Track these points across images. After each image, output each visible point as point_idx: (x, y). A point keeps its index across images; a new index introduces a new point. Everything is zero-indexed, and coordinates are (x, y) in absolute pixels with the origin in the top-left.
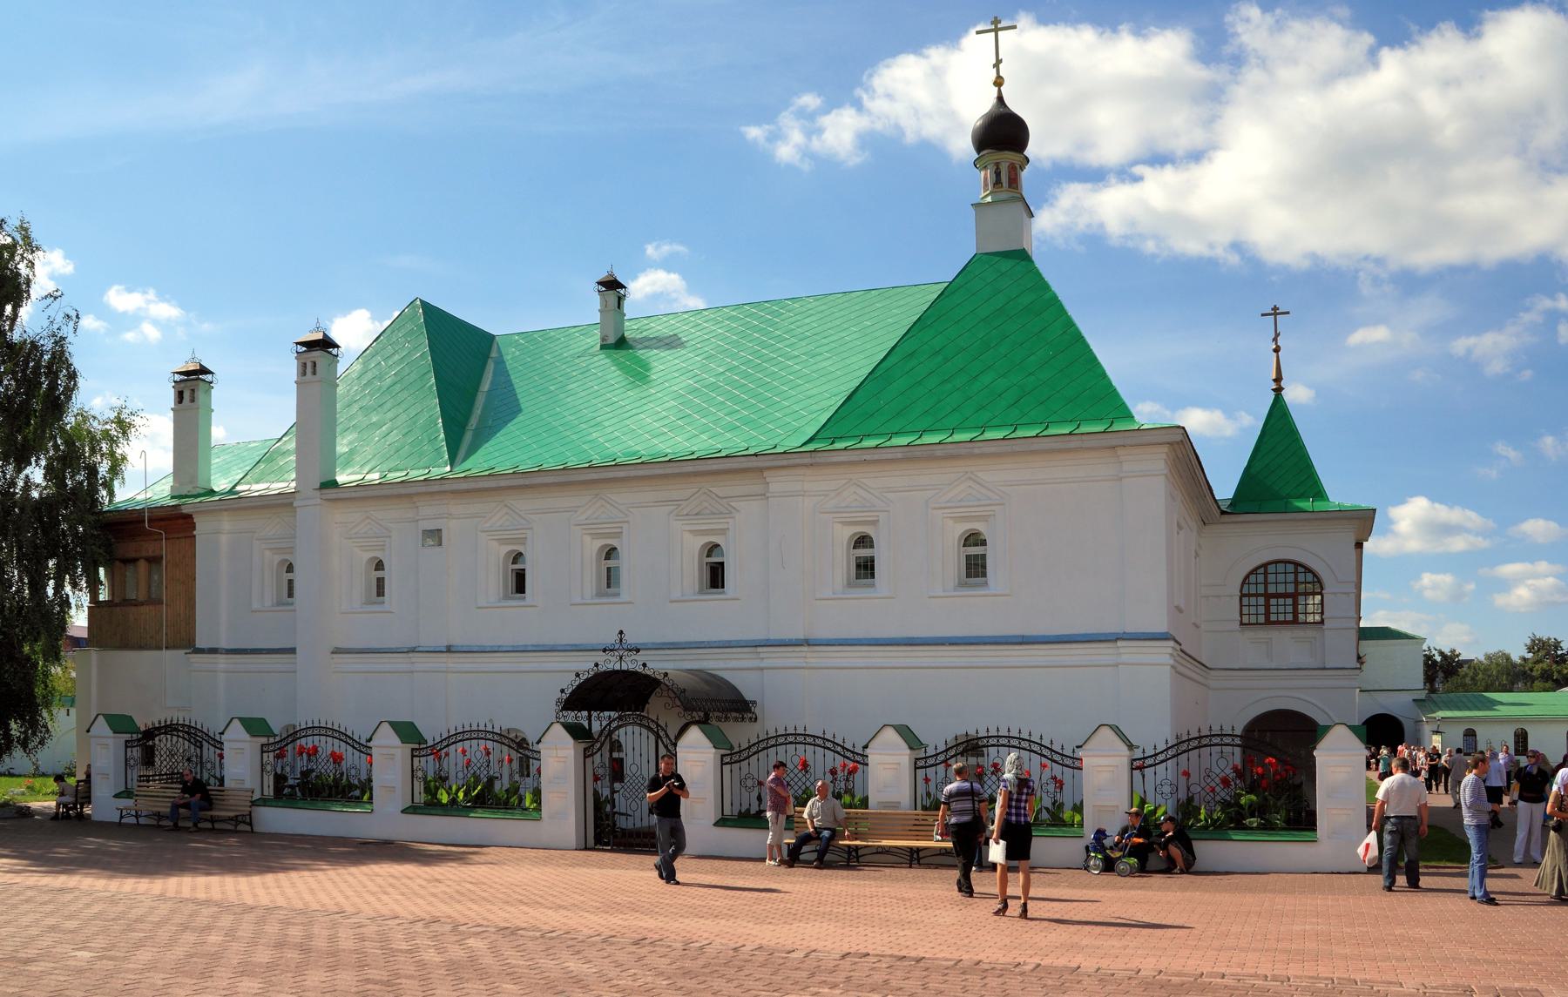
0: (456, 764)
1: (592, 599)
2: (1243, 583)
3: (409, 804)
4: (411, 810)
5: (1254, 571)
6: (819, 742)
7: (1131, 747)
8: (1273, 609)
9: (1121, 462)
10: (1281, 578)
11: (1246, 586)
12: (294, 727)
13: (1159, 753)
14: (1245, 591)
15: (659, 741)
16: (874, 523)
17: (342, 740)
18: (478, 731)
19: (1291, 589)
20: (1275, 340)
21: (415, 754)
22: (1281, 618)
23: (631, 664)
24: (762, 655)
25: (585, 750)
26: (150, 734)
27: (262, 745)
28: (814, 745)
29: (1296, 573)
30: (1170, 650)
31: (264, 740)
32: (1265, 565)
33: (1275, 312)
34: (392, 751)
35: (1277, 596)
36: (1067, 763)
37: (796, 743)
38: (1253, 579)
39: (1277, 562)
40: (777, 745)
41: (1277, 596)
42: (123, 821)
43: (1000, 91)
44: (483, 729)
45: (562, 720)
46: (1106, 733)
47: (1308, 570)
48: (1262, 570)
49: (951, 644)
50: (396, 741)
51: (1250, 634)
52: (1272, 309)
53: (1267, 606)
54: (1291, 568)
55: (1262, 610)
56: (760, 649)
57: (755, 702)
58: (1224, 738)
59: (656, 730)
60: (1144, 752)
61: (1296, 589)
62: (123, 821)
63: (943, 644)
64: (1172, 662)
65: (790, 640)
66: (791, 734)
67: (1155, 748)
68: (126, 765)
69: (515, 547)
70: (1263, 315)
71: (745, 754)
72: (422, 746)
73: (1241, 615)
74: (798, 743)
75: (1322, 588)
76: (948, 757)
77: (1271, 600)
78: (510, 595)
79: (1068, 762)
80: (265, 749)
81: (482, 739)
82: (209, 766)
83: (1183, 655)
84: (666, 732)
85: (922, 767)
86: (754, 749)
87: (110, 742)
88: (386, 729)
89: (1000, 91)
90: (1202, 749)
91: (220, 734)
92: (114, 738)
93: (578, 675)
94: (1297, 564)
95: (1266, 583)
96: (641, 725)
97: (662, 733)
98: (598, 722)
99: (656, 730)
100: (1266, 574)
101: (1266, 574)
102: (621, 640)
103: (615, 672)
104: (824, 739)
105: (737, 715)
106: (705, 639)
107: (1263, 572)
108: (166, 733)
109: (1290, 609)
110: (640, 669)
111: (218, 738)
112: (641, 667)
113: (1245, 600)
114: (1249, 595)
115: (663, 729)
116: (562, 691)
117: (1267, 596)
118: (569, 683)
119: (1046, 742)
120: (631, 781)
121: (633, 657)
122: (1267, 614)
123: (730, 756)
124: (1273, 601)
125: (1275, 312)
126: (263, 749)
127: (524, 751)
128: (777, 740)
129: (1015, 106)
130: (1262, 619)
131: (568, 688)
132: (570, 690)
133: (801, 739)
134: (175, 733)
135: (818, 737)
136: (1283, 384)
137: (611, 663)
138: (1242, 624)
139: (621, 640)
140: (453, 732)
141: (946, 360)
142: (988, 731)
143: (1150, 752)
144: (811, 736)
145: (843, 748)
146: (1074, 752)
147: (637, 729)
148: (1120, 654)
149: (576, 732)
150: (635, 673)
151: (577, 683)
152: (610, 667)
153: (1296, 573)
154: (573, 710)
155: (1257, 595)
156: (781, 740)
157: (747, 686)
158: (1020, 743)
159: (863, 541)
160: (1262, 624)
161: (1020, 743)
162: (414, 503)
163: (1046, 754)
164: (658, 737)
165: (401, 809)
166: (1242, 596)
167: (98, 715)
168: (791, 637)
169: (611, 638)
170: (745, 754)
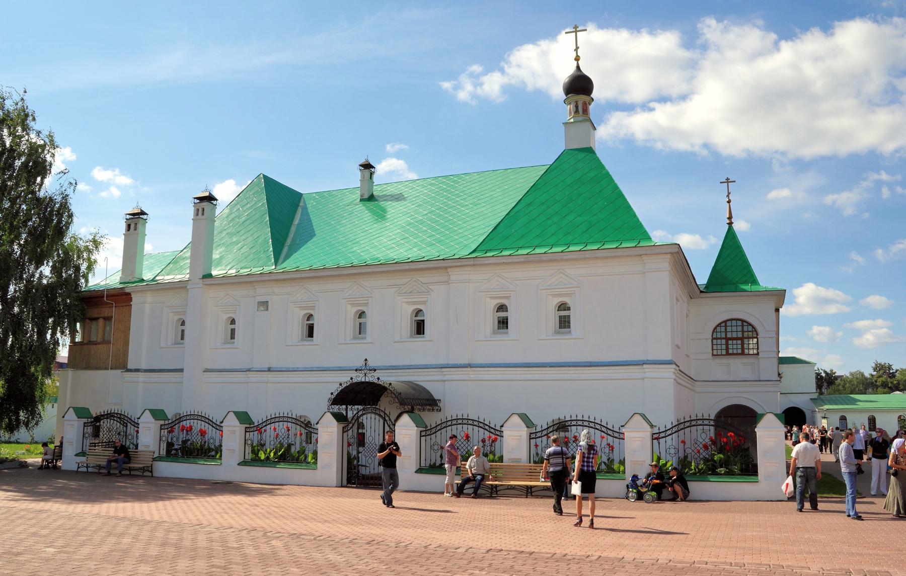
0: (270, 437)
4: (243, 464)
6: (476, 423)
8: (730, 347)
12: (180, 414)
13: (543, 430)
14: (715, 336)
16: (508, 298)
17: (481, 427)
19: (740, 335)
20: (728, 196)
22: (735, 351)
24: (444, 373)
27: (161, 425)
29: (743, 326)
30: (673, 370)
31: (162, 422)
32: (725, 322)
33: (728, 181)
39: (731, 320)
40: (452, 425)
43: (578, 64)
45: (331, 411)
46: (638, 418)
47: (749, 324)
48: (723, 324)
50: (237, 422)
52: (726, 180)
53: (727, 345)
54: (740, 323)
56: (443, 370)
57: (440, 400)
58: (704, 421)
70: (721, 183)
71: (433, 431)
73: (713, 350)
75: (757, 335)
79: (616, 435)
84: (389, 417)
86: (439, 428)
87: (76, 423)
89: (578, 64)
90: (686, 429)
93: (341, 384)
95: (726, 332)
96: (376, 414)
97: (387, 418)
100: (726, 326)
102: (366, 364)
103: (362, 383)
104: (484, 424)
108: (107, 418)
109: (740, 346)
110: (376, 381)
111: (136, 421)
113: (715, 341)
117: (727, 339)
118: (335, 389)
120: (369, 446)
121: (372, 374)
122: (727, 349)
123: (426, 432)
124: (730, 342)
125: (728, 181)
127: (308, 428)
129: (586, 71)
130: (724, 352)
132: (336, 393)
134: (112, 418)
136: (733, 220)
137: (359, 378)
138: (713, 355)
139: (366, 364)
140: (269, 418)
141: (549, 207)
142: (690, 417)
147: (373, 415)
149: (339, 417)
150: (373, 383)
151: (340, 389)
152: (359, 380)
153: (743, 326)
154: (337, 405)
156: (454, 422)
159: (502, 308)
161: (473, 422)
163: (598, 428)
164: (385, 420)
166: (713, 339)
169: (360, 363)
170: (688, 424)
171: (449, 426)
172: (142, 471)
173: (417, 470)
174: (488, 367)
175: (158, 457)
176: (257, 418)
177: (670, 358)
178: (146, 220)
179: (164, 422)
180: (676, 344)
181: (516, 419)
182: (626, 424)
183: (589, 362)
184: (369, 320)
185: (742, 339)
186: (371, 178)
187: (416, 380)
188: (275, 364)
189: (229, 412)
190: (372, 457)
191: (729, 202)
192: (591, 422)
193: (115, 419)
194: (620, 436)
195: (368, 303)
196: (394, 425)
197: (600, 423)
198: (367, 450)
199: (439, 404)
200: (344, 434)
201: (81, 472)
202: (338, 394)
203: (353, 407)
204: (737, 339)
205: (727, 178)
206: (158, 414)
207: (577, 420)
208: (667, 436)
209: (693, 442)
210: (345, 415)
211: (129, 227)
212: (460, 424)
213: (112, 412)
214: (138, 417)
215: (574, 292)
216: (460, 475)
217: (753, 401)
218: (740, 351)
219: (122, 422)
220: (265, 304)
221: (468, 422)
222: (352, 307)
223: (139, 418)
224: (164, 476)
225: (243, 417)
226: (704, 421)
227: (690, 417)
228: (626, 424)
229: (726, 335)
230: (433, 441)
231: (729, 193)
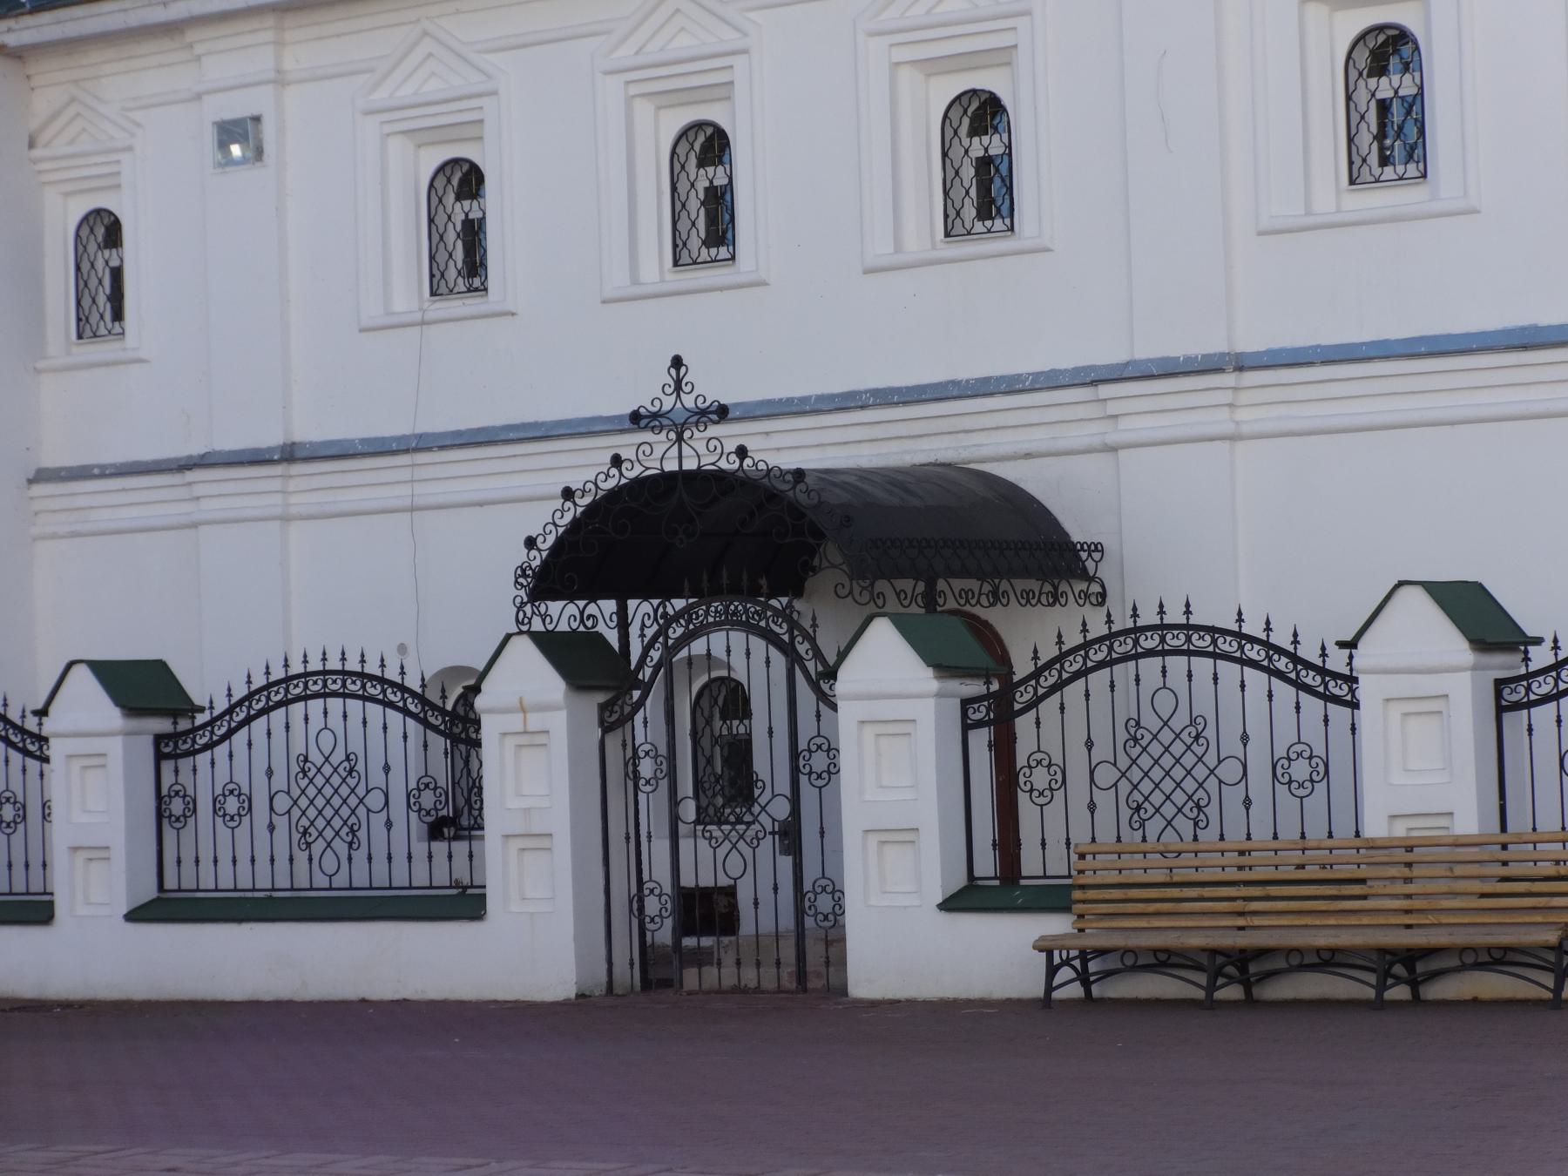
0: (270, 773)
1: (934, 248)
3: (150, 892)
9: (33, 89)
24: (1112, 408)
25: (603, 708)
27: (1500, 684)
31: (163, 725)
37: (1164, 653)
40: (1137, 657)
42: (1056, 995)
45: (537, 625)
50: (107, 714)
56: (1105, 391)
57: (1098, 548)
59: (786, 638)
62: (1056, 995)
65: (1188, 359)
72: (184, 724)
76: (1041, 691)
78: (1377, 171)
80: (1510, 696)
81: (334, 694)
82: (1040, 778)
84: (812, 640)
86: (1050, 679)
88: (84, 683)
96: (750, 628)
97: (803, 648)
99: (786, 638)
103: (666, 478)
105: (973, 584)
110: (729, 464)
111: (31, 724)
112: (733, 457)
116: (530, 543)
119: (1281, 638)
131: (545, 534)
132: (551, 540)
140: (258, 681)
145: (1267, 645)
148: (291, 476)
151: (568, 517)
154: (571, 598)
161: (1214, 642)
162: (191, 46)
165: (125, 911)
169: (648, 390)
171: (1101, 665)
172: (1202, 978)
173: (953, 897)
174: (1325, 363)
175: (158, 899)
181: (1418, 609)
184: (137, 254)
187: (985, 452)
189: (1401, 584)
190: (741, 845)
199: (1090, 565)
200: (1508, 717)
202: (560, 541)
203: (592, 609)
209: (295, 769)
210: (616, 645)
212: (1150, 653)
214: (39, 706)
222: (658, 108)
223: (1351, 645)
224: (1229, 987)
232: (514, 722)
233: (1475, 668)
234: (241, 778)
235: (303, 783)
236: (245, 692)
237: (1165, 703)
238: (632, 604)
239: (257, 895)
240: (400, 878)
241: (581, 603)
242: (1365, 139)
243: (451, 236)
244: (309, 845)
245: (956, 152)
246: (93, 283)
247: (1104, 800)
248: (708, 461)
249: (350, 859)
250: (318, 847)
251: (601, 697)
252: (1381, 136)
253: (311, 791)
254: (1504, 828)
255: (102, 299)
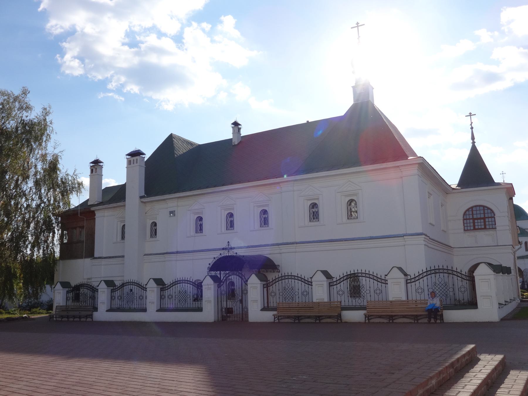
0: (279, 290)
2: (464, 215)
5: (468, 210)
7: (406, 275)
8: (476, 224)
10: (478, 212)
11: (465, 216)
14: (465, 218)
15: (243, 281)
16: (318, 199)
18: (183, 280)
19: (482, 216)
20: (471, 125)
21: (162, 290)
22: (480, 227)
23: (231, 253)
26: (77, 288)
28: (366, 277)
29: (484, 210)
30: (423, 239)
32: (472, 208)
33: (471, 115)
34: (59, 291)
35: (477, 219)
36: (383, 282)
38: (467, 213)
39: (476, 206)
41: (477, 219)
44: (132, 281)
45: (210, 274)
46: (395, 269)
47: (488, 208)
48: (471, 210)
49: (345, 241)
50: (155, 285)
51: (467, 234)
52: (469, 114)
53: (474, 223)
54: (482, 208)
55: (472, 224)
57: (279, 265)
58: (367, 275)
60: (336, 279)
61: (484, 215)
63: (342, 241)
64: (424, 243)
66: (287, 276)
67: (415, 275)
68: (66, 300)
69: (313, 201)
71: (338, 282)
74: (440, 273)
75: (494, 215)
77: (475, 220)
79: (383, 281)
81: (184, 283)
83: (430, 240)
85: (409, 283)
86: (274, 282)
87: (106, 290)
91: (145, 285)
92: (63, 290)
94: (484, 207)
95: (473, 214)
96: (237, 275)
97: (243, 278)
98: (222, 275)
100: (472, 211)
101: (472, 211)
102: (229, 245)
103: (227, 256)
105: (264, 270)
106: (374, 236)
107: (471, 210)
109: (483, 224)
110: (234, 255)
111: (145, 286)
113: (465, 221)
114: (467, 219)
115: (244, 276)
116: (209, 264)
117: (474, 219)
118: (211, 261)
119: (375, 274)
122: (474, 226)
123: (267, 285)
124: (476, 221)
125: (471, 115)
126: (68, 292)
127: (199, 285)
128: (431, 272)
130: (472, 228)
133: (290, 277)
134: (83, 287)
135: (296, 276)
137: (226, 253)
138: (465, 230)
139: (229, 245)
143: (338, 278)
144: (293, 276)
145: (301, 278)
146: (385, 278)
149: (215, 279)
153: (484, 210)
155: (469, 219)
157: (277, 261)
158: (366, 275)
160: (472, 230)
161: (294, 277)
164: (242, 279)
165: (156, 310)
166: (464, 220)
167: (57, 283)
168: (290, 242)
169: (225, 245)
170: (429, 273)
171: (179, 283)
176: (167, 281)
177: (421, 232)
178: (102, 166)
179: (113, 288)
180: (429, 223)
182: (388, 274)
183: (369, 237)
185: (484, 218)
186: (239, 132)
188: (180, 250)
191: (472, 128)
192: (367, 274)
193: (85, 287)
194: (385, 282)
195: (234, 208)
196: (247, 281)
197: (301, 277)
198: (182, 299)
199: (278, 267)
201: (296, 322)
202: (213, 264)
203: (217, 272)
204: (480, 219)
205: (470, 113)
206: (110, 283)
207: (288, 275)
208: (416, 281)
209: (433, 284)
210: (219, 277)
211: (92, 171)
212: (287, 279)
213: (83, 283)
215: (358, 193)
216: (366, 310)
217: (479, 254)
218: (483, 227)
219: (89, 289)
220: (172, 213)
221: (366, 275)
225: (159, 282)
226: (444, 271)
227: (350, 272)
228: (388, 274)
229: (473, 216)
230: (169, 293)
231: (472, 123)
232: (207, 287)
233: (327, 281)
234: (171, 293)
235: (285, 291)
236: (275, 278)
237: (288, 285)
238: (221, 272)
239: (356, 306)
240: (189, 306)
241: (215, 272)
242: (311, 216)
243: (198, 226)
244: (286, 300)
245: (262, 217)
246: (153, 231)
247: (281, 297)
248: (232, 254)
249: (363, 301)
250: (129, 303)
251: (218, 284)
252: (313, 216)
253: (180, 295)
254: (408, 299)
255: (154, 233)
